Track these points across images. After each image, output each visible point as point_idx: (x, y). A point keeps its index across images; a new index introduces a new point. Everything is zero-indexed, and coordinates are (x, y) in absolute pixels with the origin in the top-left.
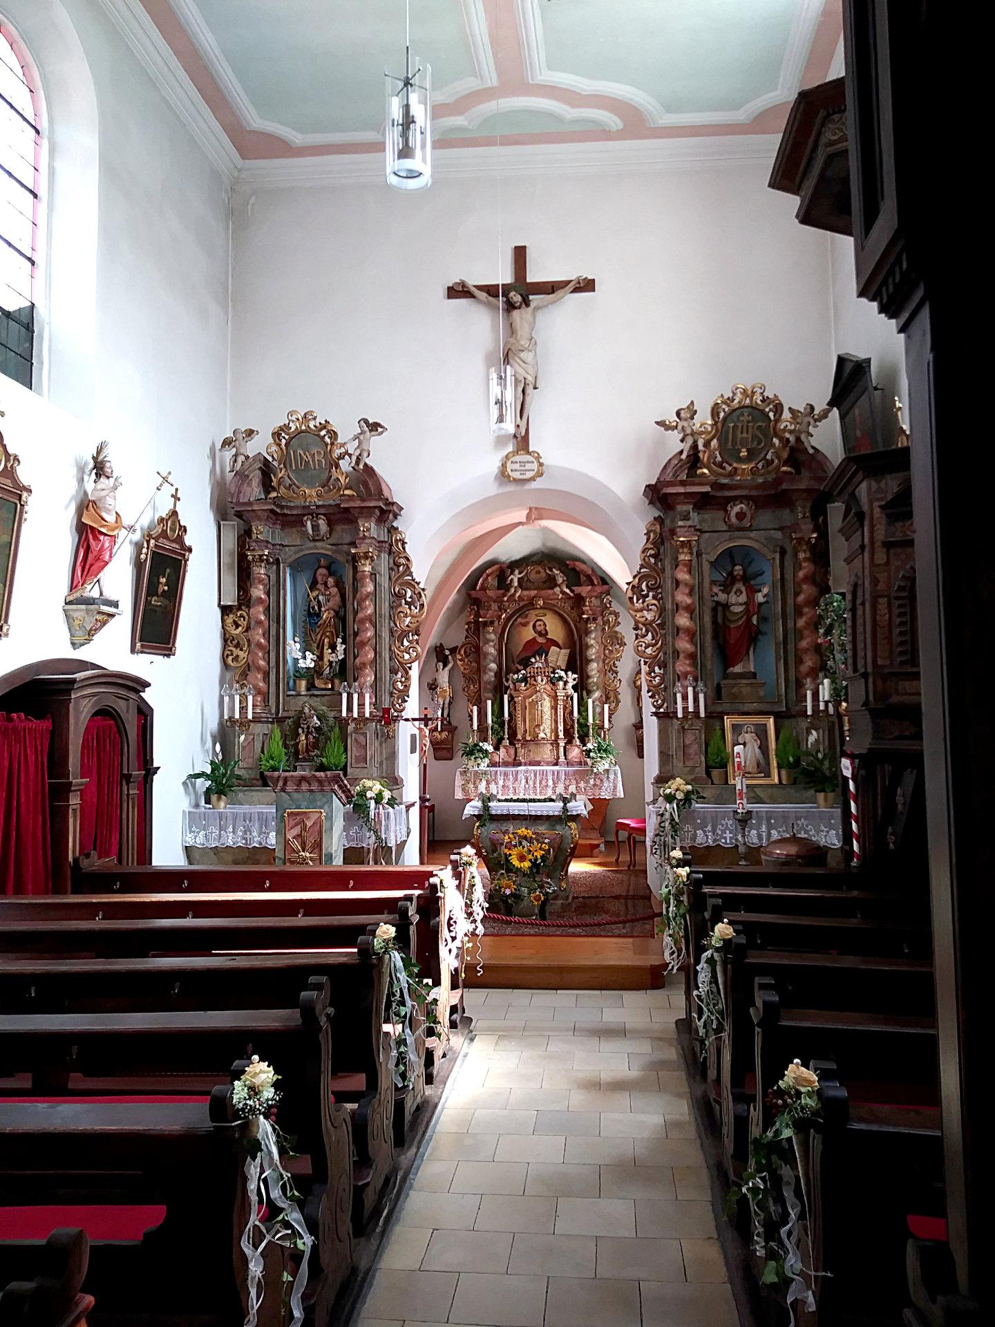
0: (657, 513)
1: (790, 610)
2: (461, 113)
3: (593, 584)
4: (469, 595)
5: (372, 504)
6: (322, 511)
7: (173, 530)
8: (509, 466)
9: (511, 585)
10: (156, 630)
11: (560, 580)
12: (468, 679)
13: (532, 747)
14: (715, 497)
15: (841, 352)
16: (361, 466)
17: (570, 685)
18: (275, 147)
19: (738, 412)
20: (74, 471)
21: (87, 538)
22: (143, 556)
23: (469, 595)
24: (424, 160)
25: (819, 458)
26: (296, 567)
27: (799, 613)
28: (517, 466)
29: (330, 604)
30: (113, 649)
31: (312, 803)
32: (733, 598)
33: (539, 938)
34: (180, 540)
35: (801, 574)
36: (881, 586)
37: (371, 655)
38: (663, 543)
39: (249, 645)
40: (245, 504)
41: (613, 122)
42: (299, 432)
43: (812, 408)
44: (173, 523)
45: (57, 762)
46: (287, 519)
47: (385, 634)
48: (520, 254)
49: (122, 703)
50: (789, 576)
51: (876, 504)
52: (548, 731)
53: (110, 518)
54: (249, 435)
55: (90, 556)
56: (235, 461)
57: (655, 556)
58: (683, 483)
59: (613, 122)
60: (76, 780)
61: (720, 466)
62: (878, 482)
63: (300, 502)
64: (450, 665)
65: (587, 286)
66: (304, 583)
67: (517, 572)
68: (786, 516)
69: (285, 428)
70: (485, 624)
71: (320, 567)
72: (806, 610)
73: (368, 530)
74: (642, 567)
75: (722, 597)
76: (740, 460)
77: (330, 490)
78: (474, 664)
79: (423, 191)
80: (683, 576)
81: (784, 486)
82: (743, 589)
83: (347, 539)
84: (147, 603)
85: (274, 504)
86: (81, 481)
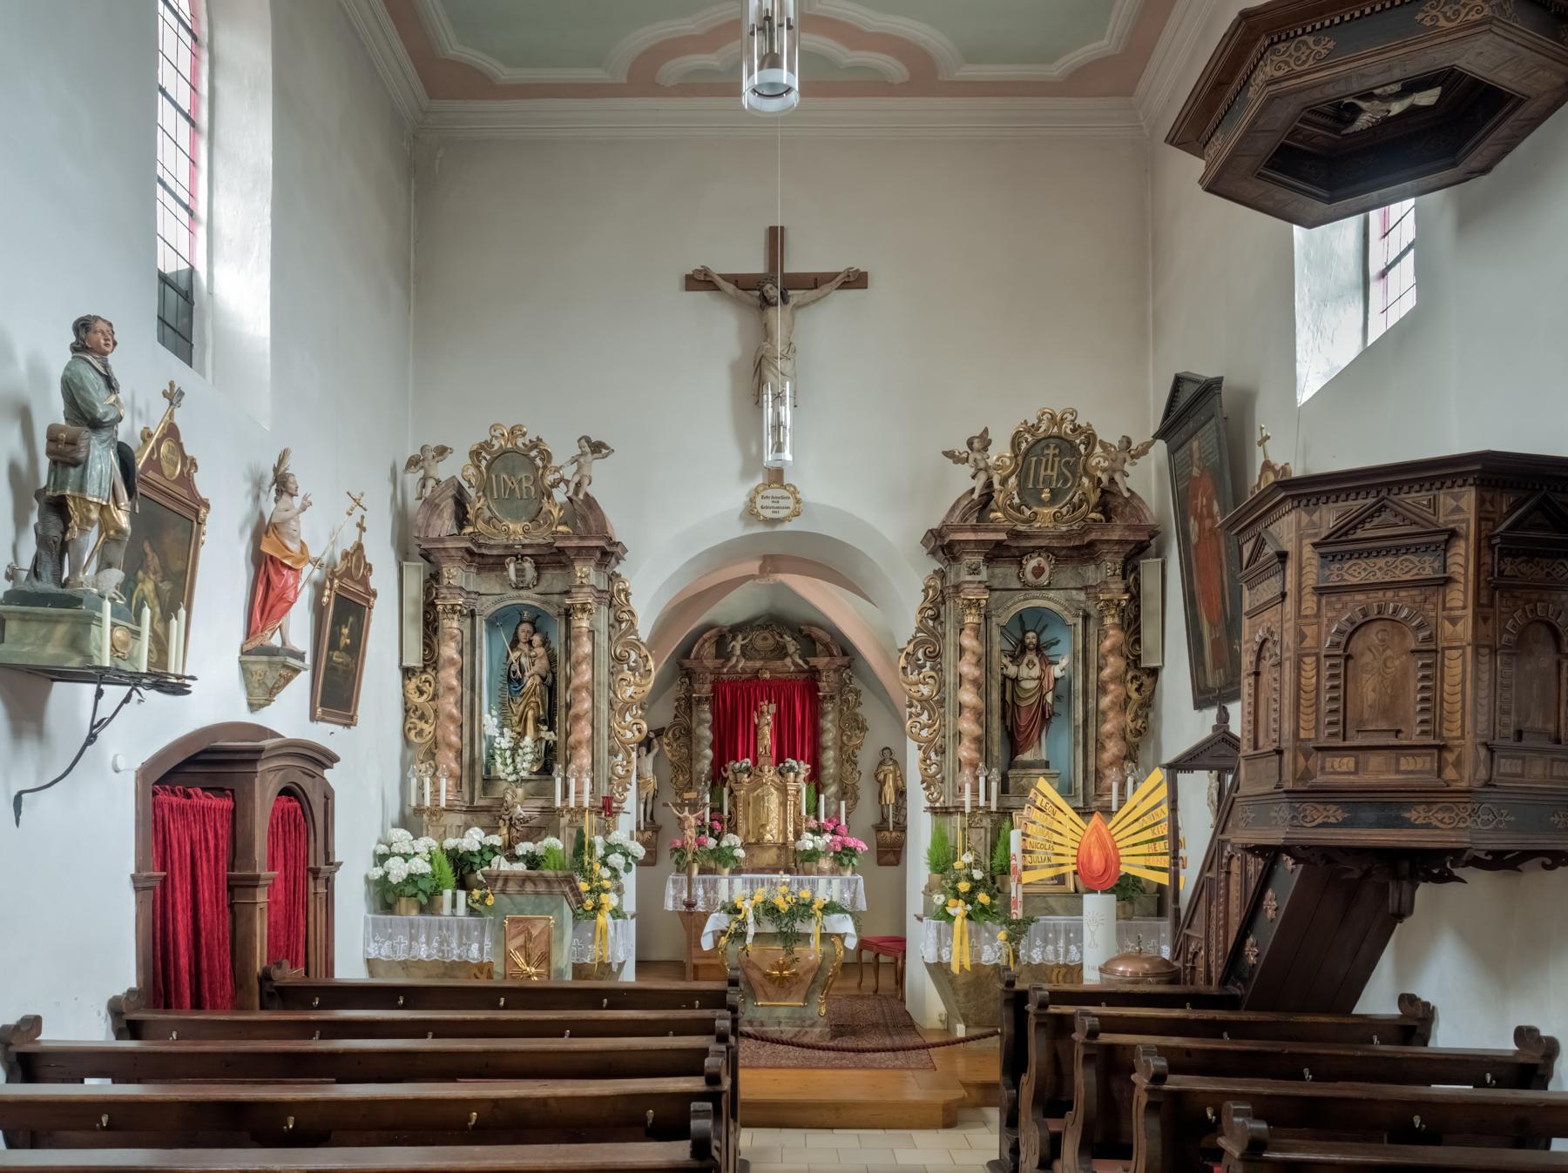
1: (1092, 687)
3: (831, 655)
4: (681, 666)
7: (358, 568)
8: (759, 502)
10: (337, 695)
11: (791, 649)
12: (677, 768)
13: (756, 851)
15: (1180, 370)
16: (581, 496)
17: (802, 776)
18: (478, 85)
19: (1043, 443)
20: (248, 486)
22: (325, 599)
23: (681, 666)
24: (791, 69)
25: (1135, 502)
26: (493, 622)
27: (1102, 689)
28: (768, 502)
29: (535, 668)
30: (290, 714)
32: (1024, 672)
33: (802, 1072)
34: (364, 581)
35: (1108, 643)
36: (1309, 642)
37: (588, 732)
38: (944, 603)
39: (436, 717)
41: (895, 68)
42: (504, 452)
43: (1129, 442)
44: (359, 560)
45: (238, 847)
46: (484, 561)
47: (604, 706)
48: (775, 238)
50: (1093, 646)
51: (1307, 542)
53: (294, 547)
56: (424, 486)
57: (936, 618)
58: (974, 529)
59: (895, 68)
62: (1311, 514)
64: (655, 751)
65: (856, 281)
66: (504, 639)
68: (1092, 574)
69: (486, 446)
70: (699, 701)
71: (522, 622)
72: (1112, 687)
74: (919, 630)
75: (1012, 670)
76: (1042, 503)
79: (786, 117)
80: (968, 641)
81: (1093, 536)
82: (1036, 661)
84: (329, 658)
86: (257, 498)
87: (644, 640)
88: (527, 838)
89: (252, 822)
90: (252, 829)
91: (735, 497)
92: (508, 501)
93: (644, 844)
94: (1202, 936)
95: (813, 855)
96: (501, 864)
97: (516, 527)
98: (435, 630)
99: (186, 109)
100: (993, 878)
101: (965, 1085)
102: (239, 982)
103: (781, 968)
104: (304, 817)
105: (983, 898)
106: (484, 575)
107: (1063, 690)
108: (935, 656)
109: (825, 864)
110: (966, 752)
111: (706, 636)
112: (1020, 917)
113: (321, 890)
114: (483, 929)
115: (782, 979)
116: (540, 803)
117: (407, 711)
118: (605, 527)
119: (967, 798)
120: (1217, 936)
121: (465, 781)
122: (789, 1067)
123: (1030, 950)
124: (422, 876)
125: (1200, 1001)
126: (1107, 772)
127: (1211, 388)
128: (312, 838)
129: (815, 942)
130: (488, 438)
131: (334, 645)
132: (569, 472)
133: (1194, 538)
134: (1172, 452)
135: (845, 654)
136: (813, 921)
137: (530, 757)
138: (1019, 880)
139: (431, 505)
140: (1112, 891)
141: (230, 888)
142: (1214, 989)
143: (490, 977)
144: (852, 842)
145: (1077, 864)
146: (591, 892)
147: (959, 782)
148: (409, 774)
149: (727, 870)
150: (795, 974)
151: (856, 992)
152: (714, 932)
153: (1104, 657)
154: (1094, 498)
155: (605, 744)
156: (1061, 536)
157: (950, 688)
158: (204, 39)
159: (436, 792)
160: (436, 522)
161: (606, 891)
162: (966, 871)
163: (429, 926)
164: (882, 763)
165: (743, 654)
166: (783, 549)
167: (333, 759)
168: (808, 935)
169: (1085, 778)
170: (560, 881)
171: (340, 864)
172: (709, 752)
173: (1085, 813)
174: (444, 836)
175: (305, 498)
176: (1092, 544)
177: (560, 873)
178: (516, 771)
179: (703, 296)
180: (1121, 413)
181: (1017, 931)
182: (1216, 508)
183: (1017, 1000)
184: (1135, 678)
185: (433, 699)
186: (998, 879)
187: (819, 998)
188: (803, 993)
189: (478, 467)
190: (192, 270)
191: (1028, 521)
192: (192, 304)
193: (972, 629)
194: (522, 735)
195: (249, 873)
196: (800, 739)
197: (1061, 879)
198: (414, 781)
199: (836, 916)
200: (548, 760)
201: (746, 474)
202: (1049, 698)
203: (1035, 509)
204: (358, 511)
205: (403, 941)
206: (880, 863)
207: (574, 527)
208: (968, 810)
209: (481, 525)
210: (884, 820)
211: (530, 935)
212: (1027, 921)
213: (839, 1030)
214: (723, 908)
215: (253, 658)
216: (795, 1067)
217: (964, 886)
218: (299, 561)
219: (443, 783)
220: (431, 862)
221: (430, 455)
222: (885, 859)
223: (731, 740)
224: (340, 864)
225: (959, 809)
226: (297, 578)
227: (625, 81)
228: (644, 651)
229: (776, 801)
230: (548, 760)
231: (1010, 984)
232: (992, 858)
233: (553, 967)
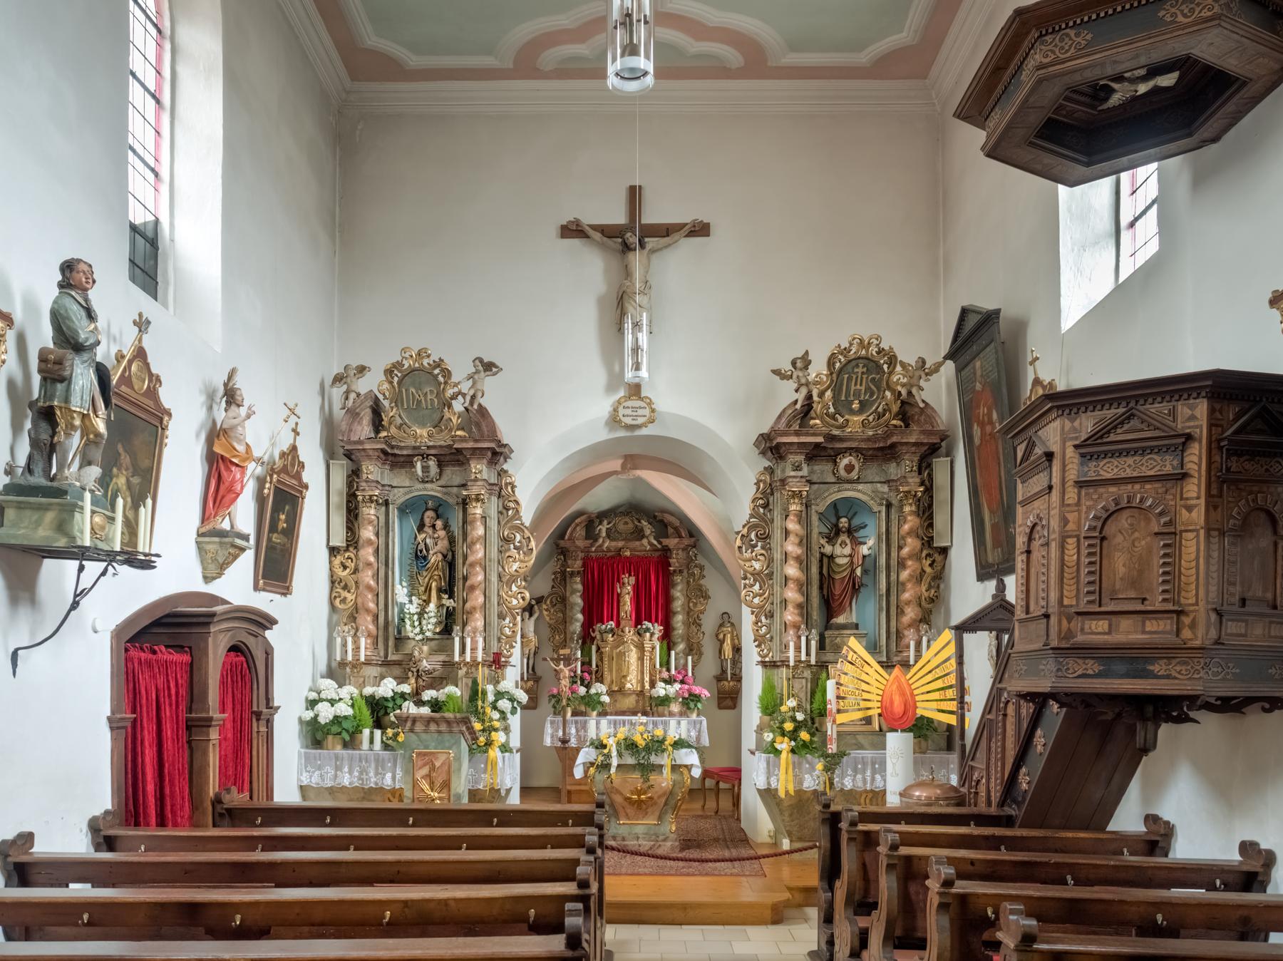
1: (894, 563)
2: (583, 41)
3: (680, 537)
4: (557, 545)
7: (293, 465)
8: (621, 411)
9: (598, 535)
10: (276, 570)
11: (648, 532)
12: (554, 629)
13: (619, 697)
14: (825, 448)
15: (965, 303)
16: (475, 407)
17: (656, 636)
18: (390, 69)
19: (854, 363)
20: (203, 398)
22: (266, 491)
23: (557, 545)
25: (929, 411)
26: (404, 510)
27: (902, 564)
28: (629, 412)
29: (438, 548)
30: (237, 585)
32: (838, 550)
34: (298, 476)
35: (906, 527)
36: (1071, 526)
37: (481, 600)
38: (772, 494)
39: (357, 587)
40: (355, 443)
41: (732, 56)
42: (412, 370)
43: (924, 362)
44: (293, 458)
45: (194, 694)
46: (396, 459)
48: (634, 195)
50: (894, 529)
52: (634, 681)
53: (241, 448)
56: (347, 398)
57: (766, 506)
58: (797, 434)
59: (732, 56)
60: (215, 714)
62: (1072, 421)
64: (536, 615)
65: (700, 230)
66: (412, 523)
68: (893, 470)
69: (397, 365)
70: (572, 574)
71: (427, 509)
72: (910, 563)
73: (480, 472)
74: (752, 516)
75: (828, 549)
76: (852, 412)
79: (644, 95)
80: (792, 525)
81: (894, 439)
82: (848, 541)
84: (269, 539)
86: (210, 408)
87: (527, 524)
88: (431, 687)
89: (207, 673)
90: (207, 679)
91: (601, 406)
93: (527, 691)
95: (665, 701)
96: (410, 708)
97: (422, 432)
98: (356, 516)
99: (152, 89)
100: (812, 719)
101: (790, 889)
102: (195, 805)
103: (639, 793)
104: (249, 669)
105: (804, 735)
107: (870, 565)
108: (765, 538)
109: (675, 708)
110: (791, 616)
111: (578, 521)
112: (835, 751)
113: (263, 729)
114: (395, 761)
116: (442, 658)
117: (333, 582)
118: (495, 431)
119: (791, 654)
120: (996, 767)
122: (646, 874)
123: (843, 778)
124: (346, 717)
125: (981, 820)
126: (906, 633)
127: (991, 318)
128: (255, 687)
129: (667, 771)
130: (400, 359)
131: (273, 528)
132: (465, 387)
133: (977, 441)
134: (959, 370)
136: (666, 755)
137: (433, 620)
138: (834, 721)
139: (353, 414)
140: (910, 730)
141: (188, 728)
143: (401, 800)
144: (697, 690)
146: (483, 730)
147: (784, 641)
148: (335, 635)
149: (595, 713)
150: (650, 798)
151: (700, 813)
152: (584, 764)
153: (904, 538)
154: (895, 408)
155: (495, 610)
156: (869, 439)
159: (357, 649)
161: (496, 730)
163: (351, 759)
164: (721, 625)
165: (608, 536)
166: (640, 449)
168: (662, 766)
169: (888, 638)
170: (458, 721)
171: (278, 708)
172: (580, 616)
173: (887, 666)
174: (363, 685)
175: (249, 408)
176: (893, 446)
177: (458, 715)
178: (422, 632)
179: (576, 243)
180: (917, 338)
181: (832, 763)
182: (995, 416)
184: (928, 555)
186: (817, 720)
187: (670, 817)
189: (391, 383)
190: (157, 222)
191: (842, 427)
192: (157, 249)
193: (796, 515)
194: (427, 602)
196: (654, 605)
197: (868, 720)
198: (339, 640)
199: (684, 750)
201: (610, 388)
204: (293, 419)
205: (330, 771)
206: (720, 707)
207: (470, 432)
208: (792, 664)
209: (393, 430)
210: (724, 672)
211: (433, 764)
212: (841, 755)
213: (687, 844)
214: (592, 744)
215: (207, 539)
216: (650, 874)
217: (789, 726)
218: (245, 460)
219: (363, 641)
220: (353, 706)
221: (352, 373)
223: (599, 606)
224: (278, 708)
225: (785, 663)
226: (243, 474)
227: (511, 66)
228: (527, 534)
229: (635, 656)
232: (812, 703)
233: (452, 792)
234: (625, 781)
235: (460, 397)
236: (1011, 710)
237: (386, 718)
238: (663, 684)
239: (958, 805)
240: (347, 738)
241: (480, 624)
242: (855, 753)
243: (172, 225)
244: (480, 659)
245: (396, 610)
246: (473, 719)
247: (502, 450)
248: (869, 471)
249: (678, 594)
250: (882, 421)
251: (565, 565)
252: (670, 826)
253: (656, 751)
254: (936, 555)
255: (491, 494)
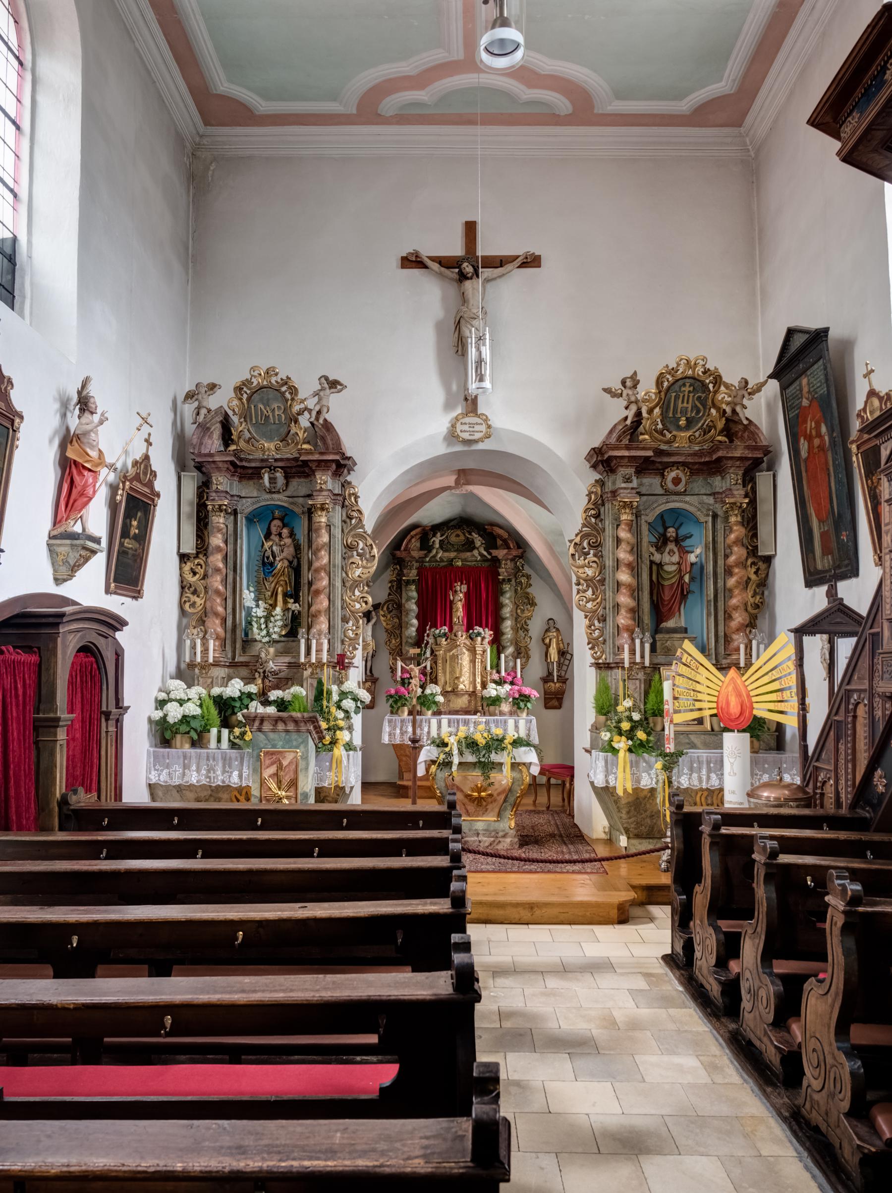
0: (598, 476)
1: (721, 570)
3: (509, 548)
5: (331, 457)
6: (280, 464)
7: (145, 474)
8: (459, 427)
10: (127, 575)
13: (452, 697)
14: (653, 462)
15: (792, 324)
16: (321, 421)
17: (487, 640)
18: (240, 114)
19: (681, 382)
20: (57, 406)
21: (70, 473)
22: (118, 498)
23: (393, 555)
25: (752, 428)
27: (729, 572)
28: (466, 428)
29: (284, 554)
30: (89, 587)
31: (288, 742)
32: (666, 558)
35: (733, 536)
37: (325, 603)
38: (603, 505)
39: (206, 592)
41: (562, 104)
43: (747, 383)
44: (146, 467)
45: (42, 694)
46: (245, 471)
47: (338, 584)
48: (470, 228)
49: (102, 640)
50: (720, 539)
52: (466, 683)
53: (94, 454)
54: (212, 389)
55: (75, 491)
56: (198, 414)
57: (597, 516)
58: (628, 448)
59: (562, 104)
60: (63, 713)
61: (661, 433)
63: (259, 455)
64: (373, 621)
65: (532, 261)
66: (260, 532)
67: (439, 534)
68: (718, 484)
69: (247, 383)
70: (408, 583)
71: (274, 519)
72: (736, 570)
73: (325, 483)
74: (584, 525)
75: (657, 557)
76: (679, 429)
77: (288, 444)
78: (396, 620)
80: (623, 534)
81: (720, 454)
82: (676, 550)
83: (303, 491)
84: (121, 544)
85: (235, 455)
86: (64, 416)
87: (369, 532)
88: (277, 687)
89: (55, 673)
90: (55, 679)
91: (440, 423)
92: (263, 424)
93: (368, 690)
94: (832, 768)
95: (496, 701)
96: (256, 708)
97: (270, 445)
98: (206, 525)
99: (13, 116)
100: (646, 719)
101: (634, 887)
102: (42, 805)
103: (479, 790)
104: (98, 670)
105: (641, 735)
106: (244, 483)
107: (698, 571)
108: (597, 546)
109: (505, 707)
110: (623, 619)
111: (413, 533)
112: (672, 751)
113: (112, 729)
114: (242, 759)
115: (480, 800)
116: (287, 659)
117: (183, 588)
118: (340, 444)
119: (626, 656)
120: (846, 768)
121: (228, 642)
122: (488, 872)
123: (679, 777)
124: (194, 717)
125: (835, 822)
126: (735, 637)
127: (819, 336)
128: (104, 687)
129: (507, 769)
130: (249, 377)
131: (125, 534)
132: (311, 403)
133: (804, 454)
134: (783, 388)
135: (519, 547)
136: (505, 753)
137: (280, 623)
138: (671, 721)
139: (203, 428)
140: (744, 731)
141: (36, 729)
142: (844, 811)
143: (248, 799)
144: (527, 691)
145: (717, 708)
146: (329, 729)
147: (618, 643)
148: (184, 637)
149: (430, 712)
150: (491, 795)
151: (532, 808)
152: (425, 761)
153: (730, 547)
154: (720, 425)
155: (339, 613)
156: (695, 454)
157: (608, 572)
158: (28, 62)
159: (205, 651)
160: (207, 441)
161: (341, 729)
162: (627, 713)
163: (199, 757)
164: (547, 630)
165: (441, 547)
166: (476, 464)
167: (123, 623)
168: (501, 764)
169: (716, 641)
170: (306, 721)
171: (128, 707)
172: (415, 622)
173: (722, 669)
174: (211, 686)
175: (102, 415)
176: (719, 459)
177: (306, 715)
178: (268, 634)
179: (416, 272)
180: (744, 360)
181: (671, 762)
182: (824, 429)
183: (688, 823)
184: (753, 563)
185: (203, 578)
186: (651, 720)
187: (509, 813)
188: (497, 810)
189: (241, 399)
190: (15, 239)
191: (669, 442)
192: (14, 265)
193: (627, 524)
194: (274, 606)
195: (52, 715)
196: (484, 613)
197: (700, 721)
198: (188, 642)
199: (523, 749)
200: (294, 626)
201: (448, 406)
202: (687, 578)
203: (674, 433)
204: (146, 429)
205: (178, 769)
206: (546, 707)
207: (315, 445)
208: (627, 665)
209: (242, 444)
210: (550, 674)
211: (281, 764)
212: (679, 754)
213: (526, 839)
214: (433, 742)
215: (58, 542)
216: (493, 872)
217: (625, 726)
218: (97, 465)
219: (211, 643)
220: (201, 706)
221: (203, 390)
222: (550, 704)
223: (434, 612)
224: (128, 707)
225: (619, 665)
226: (95, 480)
227: (355, 112)
228: (370, 541)
229: (468, 660)
230: (294, 626)
231: (680, 807)
232: (645, 703)
233: (300, 791)
234: (465, 778)
235: (306, 413)
236: (862, 711)
237: (234, 717)
238: (494, 685)
239: (808, 806)
240: (195, 737)
241: (324, 627)
242: (694, 753)
243: (29, 242)
244: (325, 661)
245: (243, 614)
246: (320, 719)
247: (346, 462)
248: (695, 485)
249: (507, 601)
250: (707, 436)
251: (400, 574)
252: (509, 823)
253: (496, 749)
254: (760, 564)
255: (335, 504)
